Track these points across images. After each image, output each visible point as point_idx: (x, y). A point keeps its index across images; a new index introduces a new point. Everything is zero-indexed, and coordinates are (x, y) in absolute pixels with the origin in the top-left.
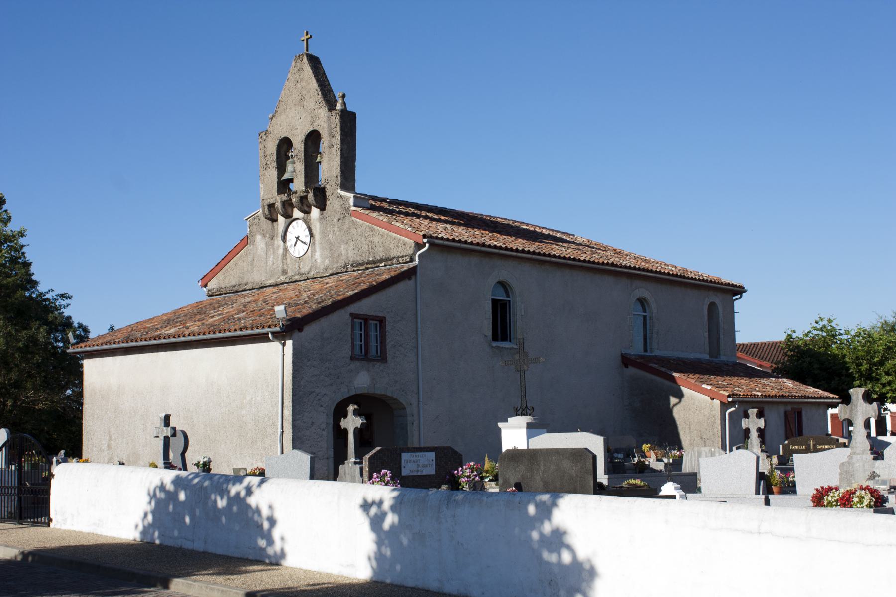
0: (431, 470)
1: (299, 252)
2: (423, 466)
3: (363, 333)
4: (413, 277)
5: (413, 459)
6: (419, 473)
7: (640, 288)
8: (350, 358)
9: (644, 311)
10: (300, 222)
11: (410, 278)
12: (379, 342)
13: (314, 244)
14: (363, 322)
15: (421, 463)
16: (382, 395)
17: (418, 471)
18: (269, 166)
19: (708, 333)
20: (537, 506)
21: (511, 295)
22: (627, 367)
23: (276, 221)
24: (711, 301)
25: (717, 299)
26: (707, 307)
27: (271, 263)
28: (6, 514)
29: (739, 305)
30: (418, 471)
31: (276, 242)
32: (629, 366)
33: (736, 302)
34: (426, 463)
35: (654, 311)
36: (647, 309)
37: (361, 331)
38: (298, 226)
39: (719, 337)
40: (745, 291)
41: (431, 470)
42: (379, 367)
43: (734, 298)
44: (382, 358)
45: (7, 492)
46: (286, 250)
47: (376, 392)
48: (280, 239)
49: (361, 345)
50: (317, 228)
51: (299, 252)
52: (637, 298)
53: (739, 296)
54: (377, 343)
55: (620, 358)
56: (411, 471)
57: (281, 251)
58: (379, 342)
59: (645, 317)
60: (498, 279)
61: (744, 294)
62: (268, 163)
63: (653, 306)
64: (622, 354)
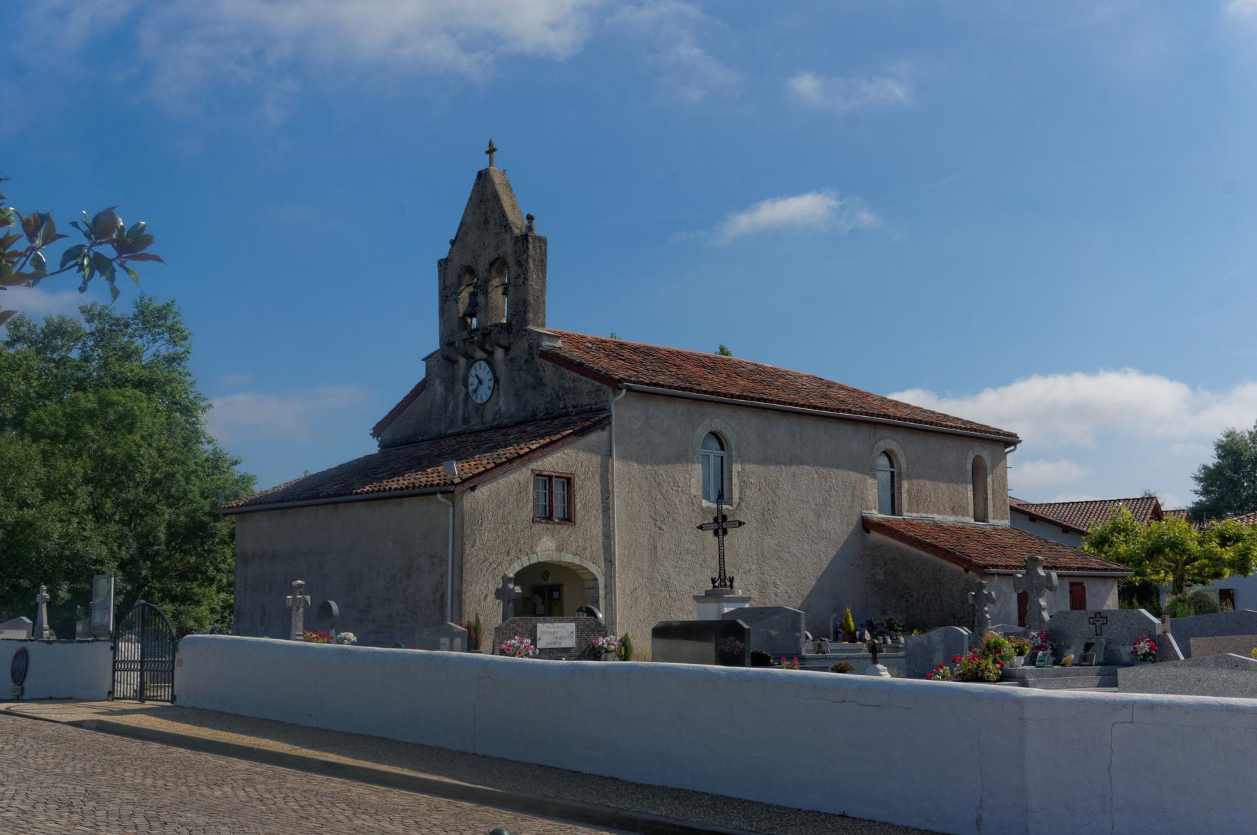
0: (570, 642)
1: (481, 398)
2: (561, 638)
3: (547, 492)
4: (607, 427)
5: (550, 630)
6: (557, 646)
7: (886, 438)
8: (531, 521)
9: (722, 449)
10: (483, 364)
11: (603, 429)
12: (566, 503)
13: (498, 390)
14: (547, 479)
15: (559, 635)
16: (568, 563)
17: (556, 643)
18: (449, 298)
19: (972, 492)
20: (148, 587)
21: (725, 448)
22: (869, 533)
23: (456, 362)
24: (976, 454)
25: (985, 453)
26: (971, 461)
27: (451, 410)
28: (132, 692)
29: (1011, 458)
30: (556, 643)
31: (457, 387)
32: (871, 531)
33: (1008, 455)
34: (565, 635)
35: (904, 466)
36: (725, 445)
37: (545, 490)
38: (480, 369)
39: (987, 497)
40: (1020, 441)
41: (570, 642)
42: (565, 530)
43: (1006, 450)
44: (568, 519)
45: (126, 667)
46: (467, 395)
47: (563, 560)
48: (460, 383)
49: (545, 506)
50: (502, 369)
51: (481, 398)
52: (882, 450)
53: (1012, 448)
54: (564, 503)
55: (860, 522)
56: (548, 644)
57: (461, 397)
58: (566, 503)
59: (892, 473)
60: (709, 430)
61: (1018, 445)
62: (448, 295)
63: (902, 460)
64: (863, 517)
